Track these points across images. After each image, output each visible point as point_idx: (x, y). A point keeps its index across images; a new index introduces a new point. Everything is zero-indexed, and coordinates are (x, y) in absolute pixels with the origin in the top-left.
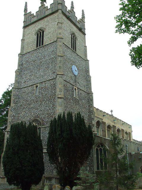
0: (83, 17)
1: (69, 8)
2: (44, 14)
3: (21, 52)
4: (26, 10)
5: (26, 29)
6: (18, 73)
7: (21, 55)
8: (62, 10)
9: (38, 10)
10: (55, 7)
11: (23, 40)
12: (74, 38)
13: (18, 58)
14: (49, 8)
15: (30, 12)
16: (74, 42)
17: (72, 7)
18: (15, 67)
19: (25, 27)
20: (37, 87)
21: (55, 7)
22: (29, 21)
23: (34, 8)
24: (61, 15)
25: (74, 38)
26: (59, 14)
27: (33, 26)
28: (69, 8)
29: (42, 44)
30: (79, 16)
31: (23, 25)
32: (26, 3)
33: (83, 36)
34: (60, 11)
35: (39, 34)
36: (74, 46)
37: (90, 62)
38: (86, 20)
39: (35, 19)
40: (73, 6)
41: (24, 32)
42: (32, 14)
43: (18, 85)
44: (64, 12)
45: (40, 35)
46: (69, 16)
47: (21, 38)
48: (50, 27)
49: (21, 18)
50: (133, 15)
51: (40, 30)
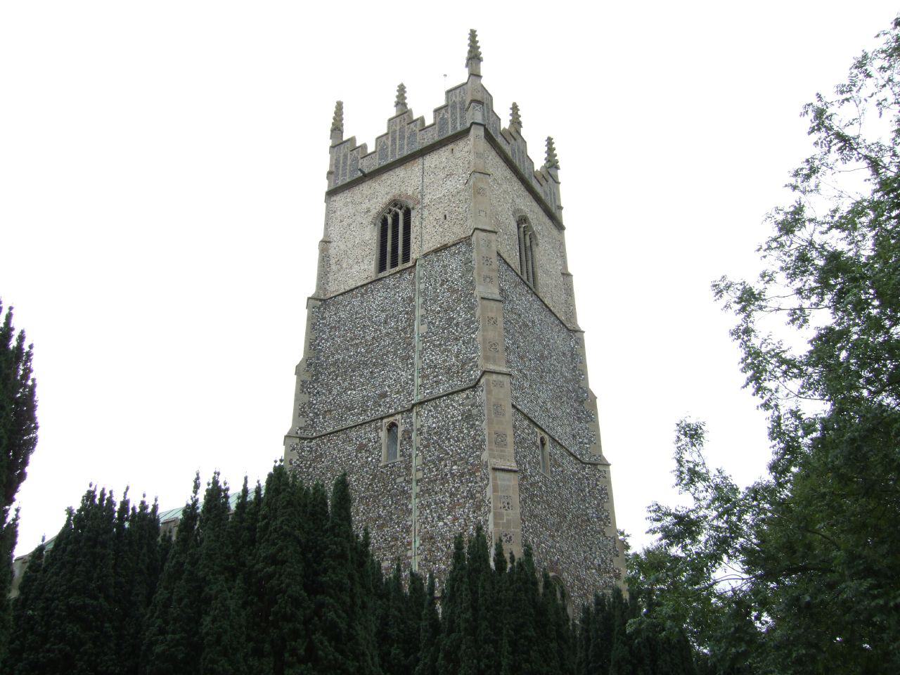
0: (552, 163)
1: (505, 124)
2: (410, 143)
3: (317, 291)
4: (337, 128)
5: (340, 199)
6: (307, 377)
7: (320, 305)
8: (484, 126)
9: (386, 131)
10: (454, 121)
11: (325, 243)
12: (528, 237)
13: (304, 313)
14: (429, 121)
15: (352, 140)
16: (524, 264)
17: (516, 122)
18: (296, 351)
19: (331, 193)
20: (392, 426)
21: (454, 121)
22: (350, 171)
23: (367, 129)
24: (483, 145)
25: (528, 237)
26: (470, 150)
27: (365, 188)
28: (505, 124)
29: (406, 257)
30: (538, 160)
31: (324, 186)
32: (339, 106)
33: (555, 232)
34: (477, 132)
35: (390, 221)
36: (527, 277)
37: (586, 337)
38: (562, 175)
39: (376, 163)
40: (518, 118)
41: (330, 213)
42: (358, 145)
43: (287, 458)
44: (491, 132)
45: (394, 229)
46: (504, 145)
47: (321, 237)
48: (441, 193)
49: (324, 162)
50: (884, 369)
51: (395, 205)
